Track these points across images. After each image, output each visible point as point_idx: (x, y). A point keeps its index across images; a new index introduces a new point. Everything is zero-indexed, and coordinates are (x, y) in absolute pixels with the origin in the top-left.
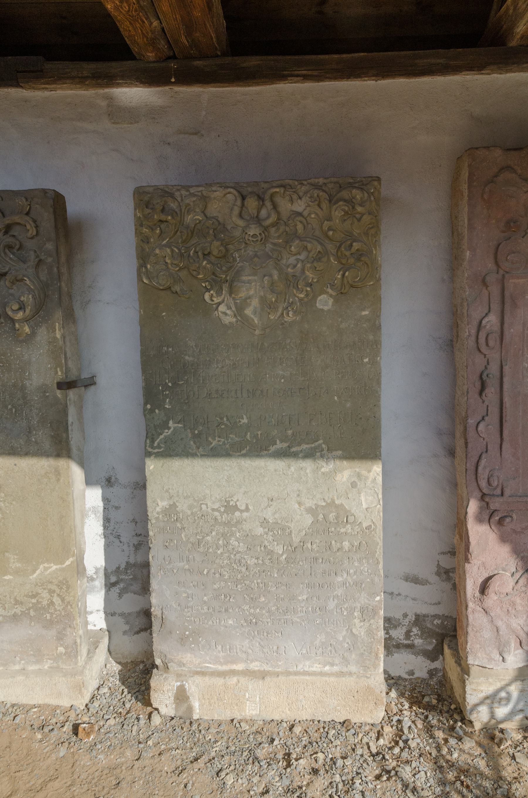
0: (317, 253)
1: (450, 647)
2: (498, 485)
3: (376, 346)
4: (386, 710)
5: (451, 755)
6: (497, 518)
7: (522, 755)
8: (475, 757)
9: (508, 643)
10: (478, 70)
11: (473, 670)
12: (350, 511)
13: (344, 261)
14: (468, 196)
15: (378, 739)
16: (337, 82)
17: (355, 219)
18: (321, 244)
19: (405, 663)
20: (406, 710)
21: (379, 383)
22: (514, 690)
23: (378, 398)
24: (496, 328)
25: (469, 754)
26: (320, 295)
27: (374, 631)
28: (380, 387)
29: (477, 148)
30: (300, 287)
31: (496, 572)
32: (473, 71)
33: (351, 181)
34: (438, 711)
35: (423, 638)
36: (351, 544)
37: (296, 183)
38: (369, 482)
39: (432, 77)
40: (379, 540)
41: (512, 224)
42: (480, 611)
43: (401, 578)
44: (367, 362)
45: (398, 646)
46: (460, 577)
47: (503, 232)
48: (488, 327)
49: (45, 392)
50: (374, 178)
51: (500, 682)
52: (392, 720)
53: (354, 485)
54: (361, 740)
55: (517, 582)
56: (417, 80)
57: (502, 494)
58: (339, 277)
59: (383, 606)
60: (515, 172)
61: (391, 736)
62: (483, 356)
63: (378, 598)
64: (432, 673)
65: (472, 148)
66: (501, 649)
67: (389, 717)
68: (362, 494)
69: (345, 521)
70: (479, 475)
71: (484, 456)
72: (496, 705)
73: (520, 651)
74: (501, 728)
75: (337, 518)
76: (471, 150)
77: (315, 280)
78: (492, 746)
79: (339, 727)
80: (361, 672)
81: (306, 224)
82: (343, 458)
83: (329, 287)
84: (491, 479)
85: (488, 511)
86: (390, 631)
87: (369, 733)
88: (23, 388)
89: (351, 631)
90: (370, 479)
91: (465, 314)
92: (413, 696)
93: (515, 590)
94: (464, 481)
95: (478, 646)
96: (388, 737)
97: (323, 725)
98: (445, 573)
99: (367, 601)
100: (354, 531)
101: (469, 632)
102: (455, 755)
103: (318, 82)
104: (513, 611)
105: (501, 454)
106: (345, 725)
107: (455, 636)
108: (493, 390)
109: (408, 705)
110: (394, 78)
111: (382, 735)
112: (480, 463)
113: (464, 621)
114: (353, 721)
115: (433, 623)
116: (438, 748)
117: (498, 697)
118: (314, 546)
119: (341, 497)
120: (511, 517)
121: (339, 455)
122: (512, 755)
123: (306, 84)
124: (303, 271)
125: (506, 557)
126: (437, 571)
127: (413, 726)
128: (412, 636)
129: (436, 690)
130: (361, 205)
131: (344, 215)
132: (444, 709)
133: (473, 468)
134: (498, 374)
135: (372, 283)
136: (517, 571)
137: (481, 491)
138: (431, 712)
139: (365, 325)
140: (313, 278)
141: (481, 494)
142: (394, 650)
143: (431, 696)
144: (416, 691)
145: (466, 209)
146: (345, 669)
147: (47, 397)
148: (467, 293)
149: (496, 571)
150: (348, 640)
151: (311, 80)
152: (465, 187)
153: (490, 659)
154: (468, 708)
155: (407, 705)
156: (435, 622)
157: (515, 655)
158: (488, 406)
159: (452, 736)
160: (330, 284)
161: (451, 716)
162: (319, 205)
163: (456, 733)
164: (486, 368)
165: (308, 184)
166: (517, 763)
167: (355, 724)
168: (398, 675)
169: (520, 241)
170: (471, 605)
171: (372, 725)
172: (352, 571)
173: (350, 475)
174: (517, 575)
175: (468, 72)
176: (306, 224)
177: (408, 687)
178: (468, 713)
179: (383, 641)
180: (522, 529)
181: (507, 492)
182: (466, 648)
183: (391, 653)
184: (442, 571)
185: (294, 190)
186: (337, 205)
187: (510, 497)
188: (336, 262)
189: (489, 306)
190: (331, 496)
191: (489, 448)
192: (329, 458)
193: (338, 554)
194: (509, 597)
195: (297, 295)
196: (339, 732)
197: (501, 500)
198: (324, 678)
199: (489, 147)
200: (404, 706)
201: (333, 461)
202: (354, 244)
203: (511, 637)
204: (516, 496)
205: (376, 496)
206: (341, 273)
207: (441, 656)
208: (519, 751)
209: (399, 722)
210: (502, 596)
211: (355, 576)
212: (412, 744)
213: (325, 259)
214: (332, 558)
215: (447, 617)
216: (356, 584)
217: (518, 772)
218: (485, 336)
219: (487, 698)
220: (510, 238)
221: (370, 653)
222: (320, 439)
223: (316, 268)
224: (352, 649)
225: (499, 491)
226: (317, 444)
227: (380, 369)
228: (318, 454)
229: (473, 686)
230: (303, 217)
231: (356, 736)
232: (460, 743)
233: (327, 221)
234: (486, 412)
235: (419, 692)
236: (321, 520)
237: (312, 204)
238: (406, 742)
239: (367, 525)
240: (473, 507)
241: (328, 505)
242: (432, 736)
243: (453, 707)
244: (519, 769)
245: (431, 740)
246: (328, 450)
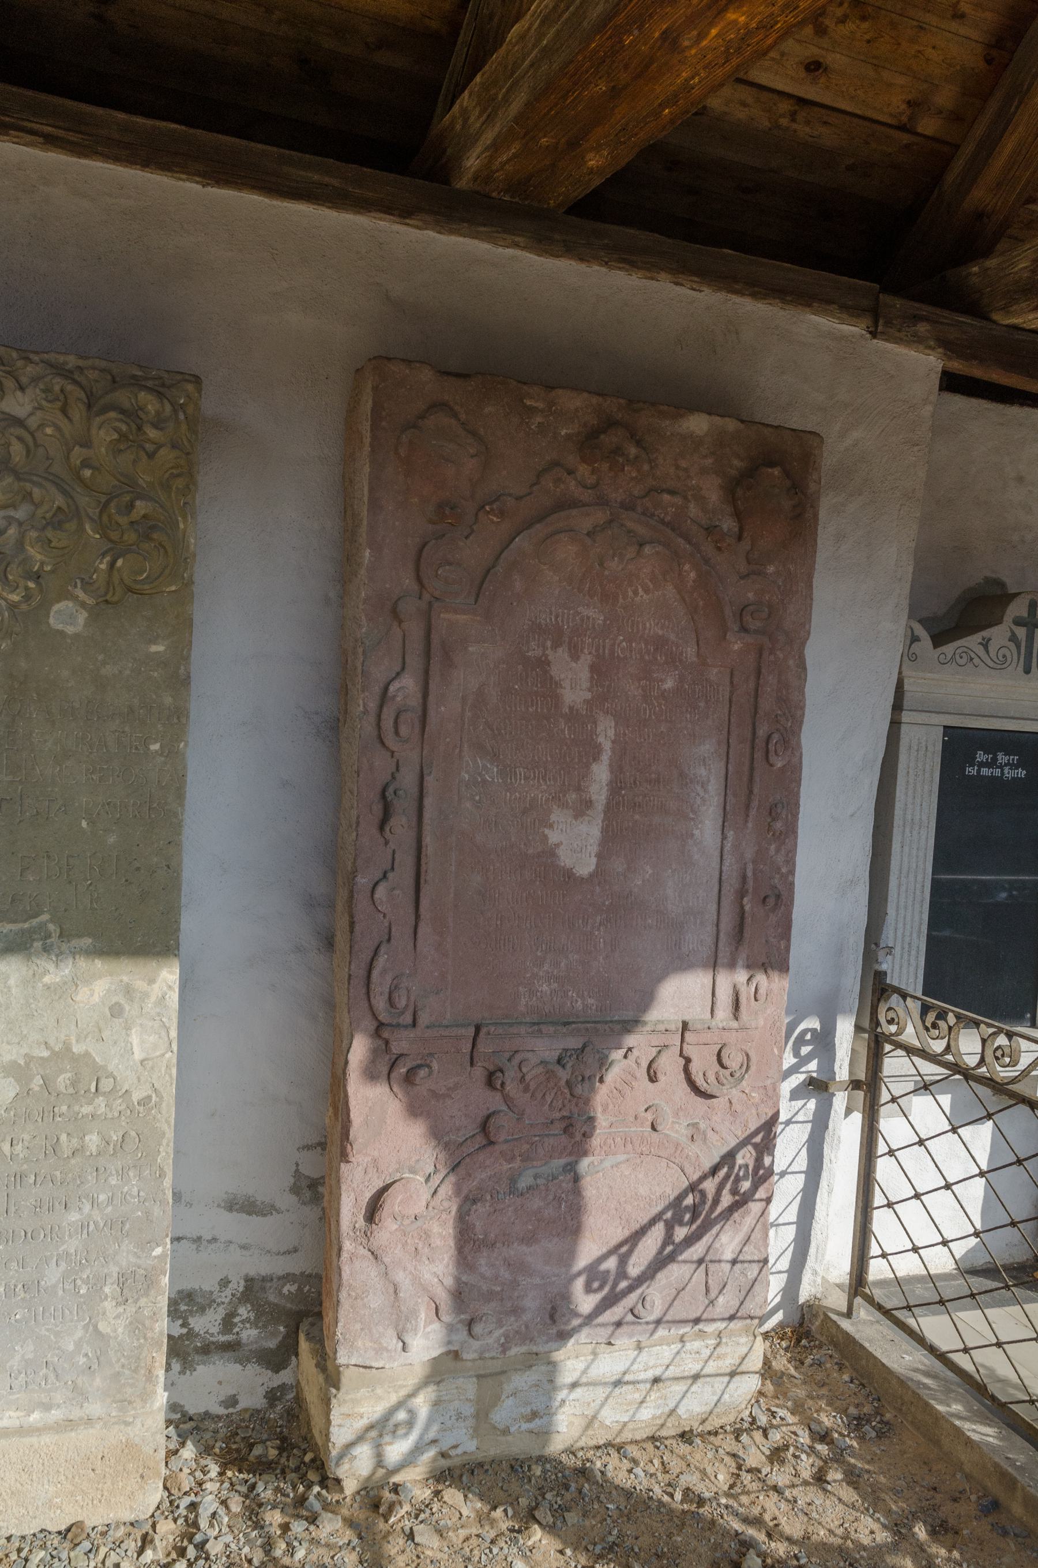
0: (54, 510)
1: (309, 1338)
2: (407, 1006)
3: (178, 718)
4: (165, 1488)
5: (292, 1555)
6: (404, 1070)
7: (426, 1527)
8: (338, 1550)
9: (414, 1313)
10: (400, 216)
11: (347, 1377)
12: (104, 1068)
13: (114, 535)
14: (371, 445)
15: (141, 1552)
16: (121, 169)
17: (142, 453)
18: (64, 492)
19: (220, 1383)
20: (211, 1480)
21: (180, 796)
22: (422, 1404)
23: (177, 828)
24: (415, 702)
25: (327, 1545)
26: (58, 601)
27: (147, 1322)
28: (182, 805)
29: (389, 359)
30: (10, 577)
31: (397, 1176)
32: (392, 215)
33: (140, 373)
34: (278, 1471)
35: (260, 1325)
36: (103, 1138)
37: (14, 355)
38: (149, 1005)
39: (316, 207)
40: (165, 1127)
41: (447, 511)
42: (364, 1257)
43: (219, 1206)
44: (156, 752)
45: (206, 1350)
46: (331, 1193)
47: (431, 522)
48: (399, 699)
50: (187, 377)
51: (396, 1392)
52: (178, 1507)
53: (116, 1011)
54: (103, 1562)
55: (435, 1192)
56: (285, 204)
57: (414, 1024)
58: (103, 566)
59: (168, 1266)
60: (455, 415)
61: (171, 1540)
62: (389, 754)
63: (158, 1251)
64: (273, 1396)
65: (380, 357)
66: (400, 1327)
67: (171, 1502)
68: (134, 1031)
69: (93, 1090)
70: (372, 986)
71: (383, 949)
72: (387, 1438)
73: (436, 1326)
74: (394, 1484)
75: (74, 1083)
76: (381, 360)
77: (48, 568)
78: (373, 1520)
79: (56, 1542)
80: (114, 1414)
81: (31, 443)
82: (95, 953)
83: (79, 585)
84: (395, 995)
85: (387, 1057)
86: (191, 1320)
87: (122, 1542)
89: (96, 1327)
90: (153, 999)
91: (359, 670)
92: (230, 1448)
93: (430, 1208)
94: (345, 1000)
95: (358, 1326)
96: (164, 1542)
97: (17, 1545)
98: (309, 1187)
99: (132, 1259)
100: (111, 1110)
101: (342, 1300)
102: (300, 1554)
103: (79, 158)
104: (426, 1250)
105: (415, 946)
106: (70, 1536)
107: (319, 1315)
108: (404, 820)
109: (218, 1469)
110: (240, 190)
111: (152, 1541)
112: (375, 963)
113: (335, 1279)
114: (89, 1524)
115: (280, 1292)
116: (268, 1546)
117: (392, 1422)
118: (18, 1148)
119: (86, 1037)
120: (429, 1067)
121: (85, 947)
122: (408, 1531)
123: (50, 154)
124: (20, 544)
125: (418, 1146)
126: (295, 1184)
127: (222, 1511)
128: (235, 1325)
129: (278, 1430)
130: (155, 426)
131: (118, 441)
132: (291, 1465)
133: (363, 973)
134: (414, 791)
135: (173, 588)
136: (436, 1170)
137: (376, 1019)
138: (265, 1477)
139: (156, 674)
140: (42, 564)
141: (375, 1024)
142: (197, 1358)
143: (268, 1443)
144: (238, 1439)
145: (367, 469)
146: (76, 1414)
148: (364, 630)
149: (399, 1174)
150: (86, 1348)
151: (61, 148)
152: (366, 428)
153: (380, 1350)
154: (334, 1453)
155: (214, 1470)
156: (285, 1290)
157: (426, 1336)
158: (394, 852)
159: (298, 1517)
160: (82, 580)
161: (303, 1478)
162: (64, 411)
163: (307, 1510)
164: (393, 777)
165: (42, 361)
166: (417, 1544)
167: (93, 1529)
168: (202, 1410)
169: (461, 544)
170: (348, 1246)
171: (132, 1524)
172: (102, 1197)
173: (108, 991)
174: (436, 1180)
175: (382, 215)
176: (31, 443)
177: (223, 1432)
178: (333, 1464)
179: (166, 1341)
180: (448, 1089)
181: (424, 1019)
182: (335, 1333)
183: (192, 1366)
184: (304, 1183)
185: (8, 369)
186: (102, 418)
187: (428, 1027)
188: (98, 536)
189: (404, 658)
190: (63, 1037)
191: (393, 933)
192: (61, 953)
193: (73, 1161)
194: (419, 1223)
195: (5, 594)
196: (54, 1553)
197: (411, 1034)
198: (27, 1440)
199: (410, 361)
200: (209, 1472)
201: (71, 960)
202: (138, 503)
203: (420, 1301)
204: (439, 1026)
205: (163, 1033)
206: (108, 559)
207: (293, 1358)
208: (421, 1522)
209: (193, 1506)
210: (406, 1222)
211: (110, 1208)
212: (214, 1548)
213: (72, 526)
214: (58, 1173)
215: (310, 1276)
216: (110, 1224)
217: (417, 1561)
218: (393, 716)
219: (371, 1427)
220: (444, 535)
221: (136, 1371)
222: (43, 913)
223: (50, 541)
224: (95, 1366)
225: (408, 1018)
226: (35, 922)
227: (185, 767)
228: (38, 945)
229: (344, 1409)
230: (26, 428)
231: (91, 1556)
232: (312, 1528)
233: (81, 446)
234: (390, 862)
235: (245, 1438)
236: (37, 1089)
237: (49, 405)
238: (201, 1546)
239: (141, 1097)
240: (359, 1050)
241: (55, 1055)
242: (258, 1525)
243: (308, 1458)
244: (418, 1557)
245: (254, 1533)
246: (61, 936)
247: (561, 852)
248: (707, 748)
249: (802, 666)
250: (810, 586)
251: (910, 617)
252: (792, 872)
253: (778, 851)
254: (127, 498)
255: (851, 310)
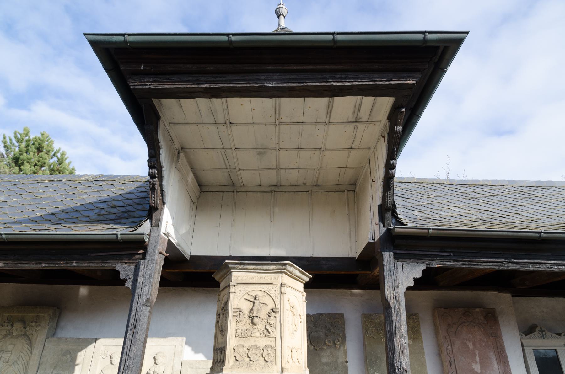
24: (451, 349)
49: (343, 364)
88: (337, 362)
134: (454, 361)
147: (343, 365)
247: (475, 369)
248: (492, 353)
249: (502, 340)
250: (500, 329)
251: (520, 332)
252: (511, 372)
253: (507, 369)
254: (414, 328)
255: (495, 290)
